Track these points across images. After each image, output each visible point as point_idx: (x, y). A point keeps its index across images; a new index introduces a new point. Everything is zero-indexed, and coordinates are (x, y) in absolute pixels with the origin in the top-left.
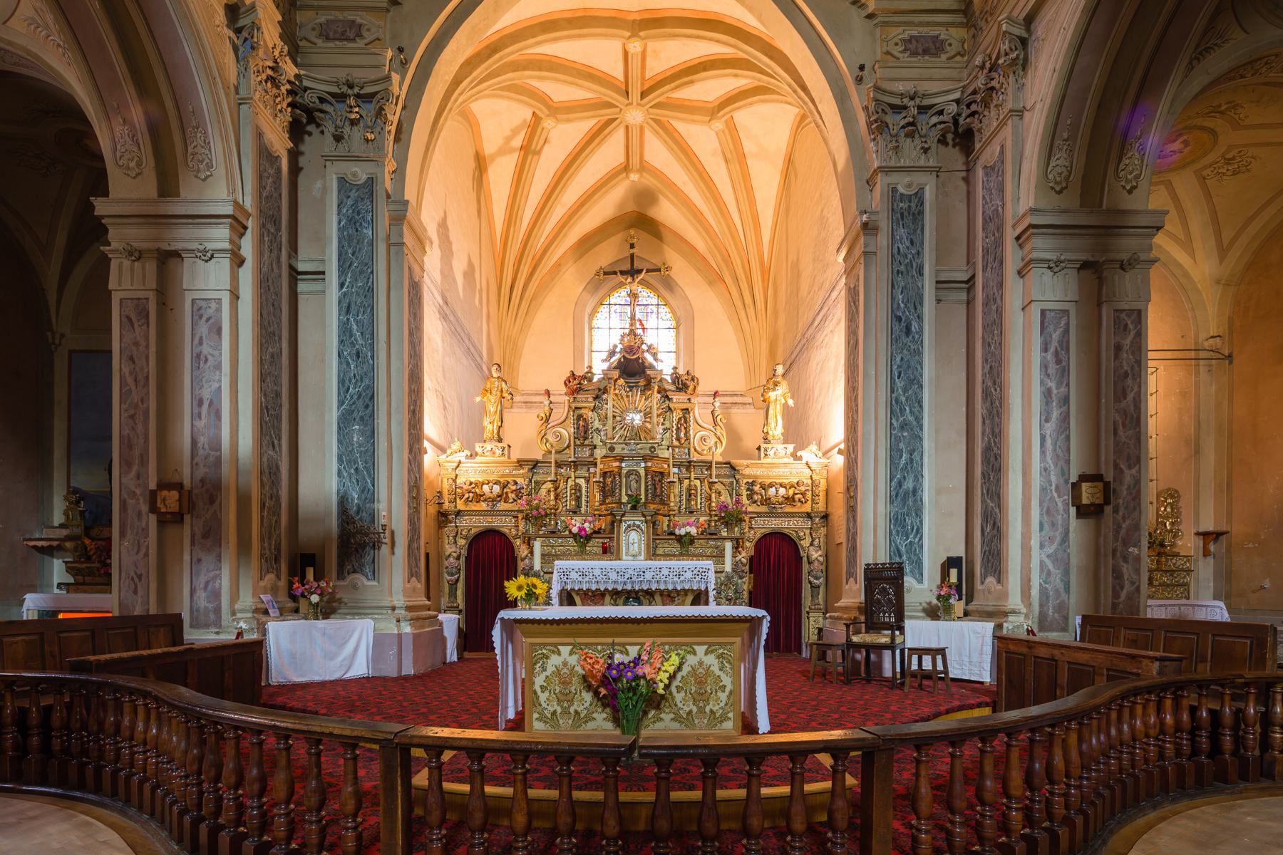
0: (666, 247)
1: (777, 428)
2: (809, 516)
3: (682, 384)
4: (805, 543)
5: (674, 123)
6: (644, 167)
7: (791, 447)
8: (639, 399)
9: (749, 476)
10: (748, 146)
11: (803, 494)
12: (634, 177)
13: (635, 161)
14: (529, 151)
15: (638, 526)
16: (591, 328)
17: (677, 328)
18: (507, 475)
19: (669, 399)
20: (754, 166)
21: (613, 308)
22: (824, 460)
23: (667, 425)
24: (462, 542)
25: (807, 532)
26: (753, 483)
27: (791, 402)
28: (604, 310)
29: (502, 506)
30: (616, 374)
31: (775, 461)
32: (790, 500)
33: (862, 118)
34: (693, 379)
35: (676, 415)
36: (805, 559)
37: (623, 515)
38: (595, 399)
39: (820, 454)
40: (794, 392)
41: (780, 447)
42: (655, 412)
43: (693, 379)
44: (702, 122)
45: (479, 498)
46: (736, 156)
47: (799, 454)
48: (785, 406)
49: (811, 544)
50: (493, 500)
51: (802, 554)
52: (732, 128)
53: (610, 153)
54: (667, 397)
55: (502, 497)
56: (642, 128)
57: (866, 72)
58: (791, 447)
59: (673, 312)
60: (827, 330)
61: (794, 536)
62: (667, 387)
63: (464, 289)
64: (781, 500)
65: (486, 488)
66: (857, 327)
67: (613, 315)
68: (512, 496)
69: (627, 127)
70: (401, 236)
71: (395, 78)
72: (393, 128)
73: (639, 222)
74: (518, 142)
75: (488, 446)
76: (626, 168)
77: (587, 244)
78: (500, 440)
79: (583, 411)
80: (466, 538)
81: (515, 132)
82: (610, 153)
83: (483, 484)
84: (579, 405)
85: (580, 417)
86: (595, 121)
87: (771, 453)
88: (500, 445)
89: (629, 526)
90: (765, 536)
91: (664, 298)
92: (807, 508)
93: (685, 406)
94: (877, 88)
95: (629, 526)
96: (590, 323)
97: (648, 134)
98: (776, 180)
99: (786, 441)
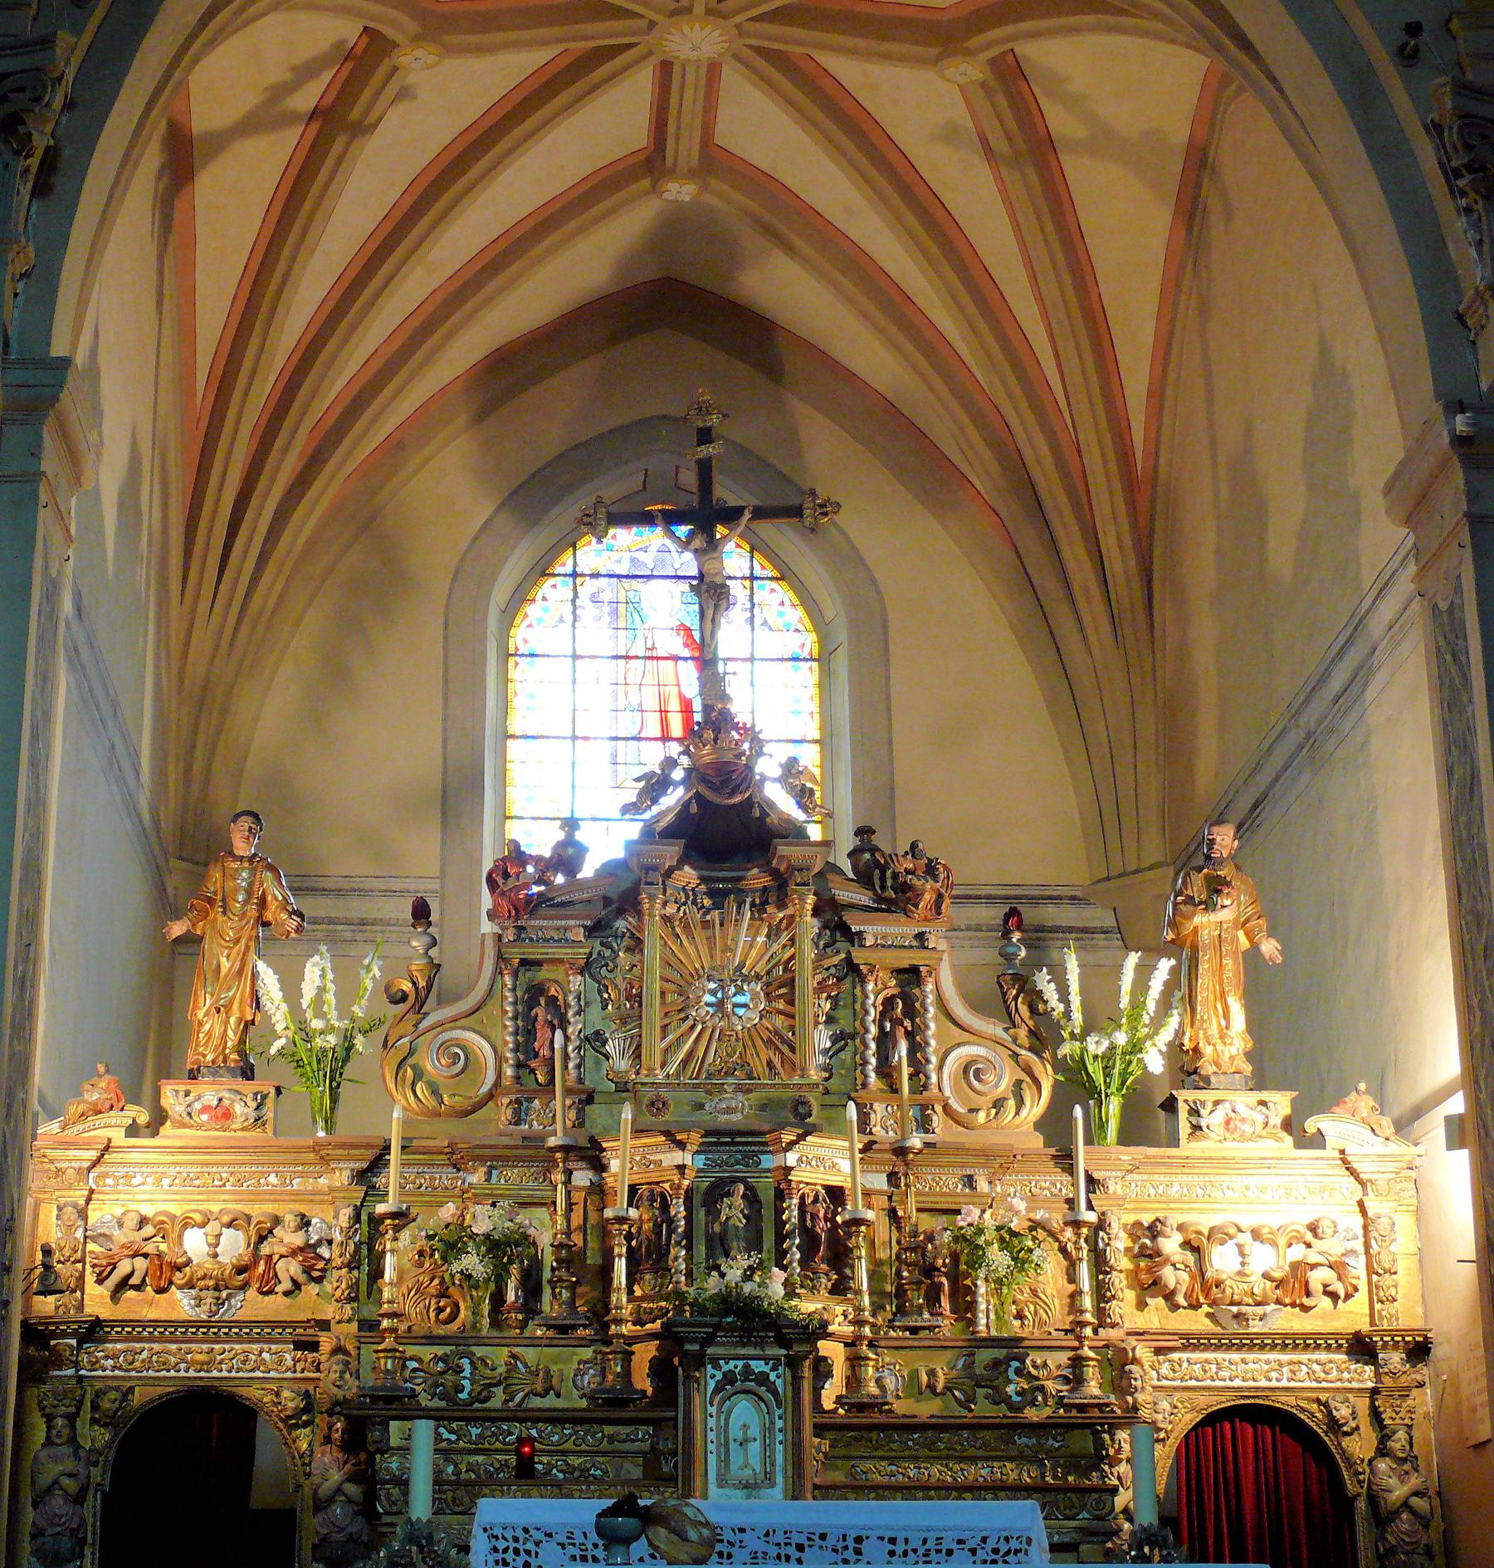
0: (790, 397)
1: (1227, 1035)
2: (1361, 1348)
3: (888, 879)
4: (1360, 1445)
5: (823, 58)
6: (714, 161)
7: (1281, 1103)
8: (749, 942)
9: (1141, 1204)
10: (1059, 121)
11: (1338, 1267)
12: (680, 191)
13: (684, 148)
14: (335, 125)
15: (762, 1379)
16: (506, 655)
17: (824, 658)
18: (275, 1196)
19: (854, 938)
20: (1085, 176)
21: (588, 587)
22: (1398, 1148)
23: (845, 1022)
24: (96, 1437)
25: (1363, 1404)
26: (1154, 1230)
27: (1269, 947)
28: (553, 594)
29: (250, 1305)
30: (671, 852)
31: (1233, 1149)
32: (1293, 1286)
33: (1426, 152)
34: (931, 870)
35: (874, 993)
36: (1361, 1505)
37: (709, 1340)
38: (590, 932)
39: (1387, 1124)
40: (1274, 913)
41: (1244, 1101)
42: (808, 979)
43: (931, 870)
44: (919, 61)
45: (167, 1273)
46: (1030, 148)
47: (1311, 1125)
48: (1253, 957)
49: (1382, 1451)
50: (226, 1284)
51: (1351, 1487)
52: (1010, 75)
53: (612, 120)
54: (843, 929)
55: (249, 1273)
56: (713, 71)
57: (1426, 37)
58: (1281, 1103)
59: (807, 601)
60: (1371, 693)
61: (1315, 1422)
62: (844, 895)
63: (117, 553)
64: (1260, 1287)
65: (195, 1244)
66: (1471, 730)
67: (587, 611)
68: (289, 1269)
69: (666, 67)
70: (35, 454)
71: (64, 38)
72: (34, 162)
73: (681, 309)
74: (306, 99)
75: (208, 1093)
76: (651, 164)
77: (507, 374)
78: (248, 1073)
79: (544, 974)
80: (107, 1420)
81: (305, 72)
82: (612, 120)
83: (187, 1223)
84: (535, 953)
85: (536, 992)
86: (560, 48)
87: (1213, 1120)
88: (249, 1087)
89: (729, 1378)
90: (1213, 1419)
91: (772, 556)
92: (1354, 1316)
93: (906, 960)
94: (1462, 88)
95: (729, 1378)
96: (504, 636)
97: (732, 79)
98: (1159, 223)
99: (1259, 1082)
